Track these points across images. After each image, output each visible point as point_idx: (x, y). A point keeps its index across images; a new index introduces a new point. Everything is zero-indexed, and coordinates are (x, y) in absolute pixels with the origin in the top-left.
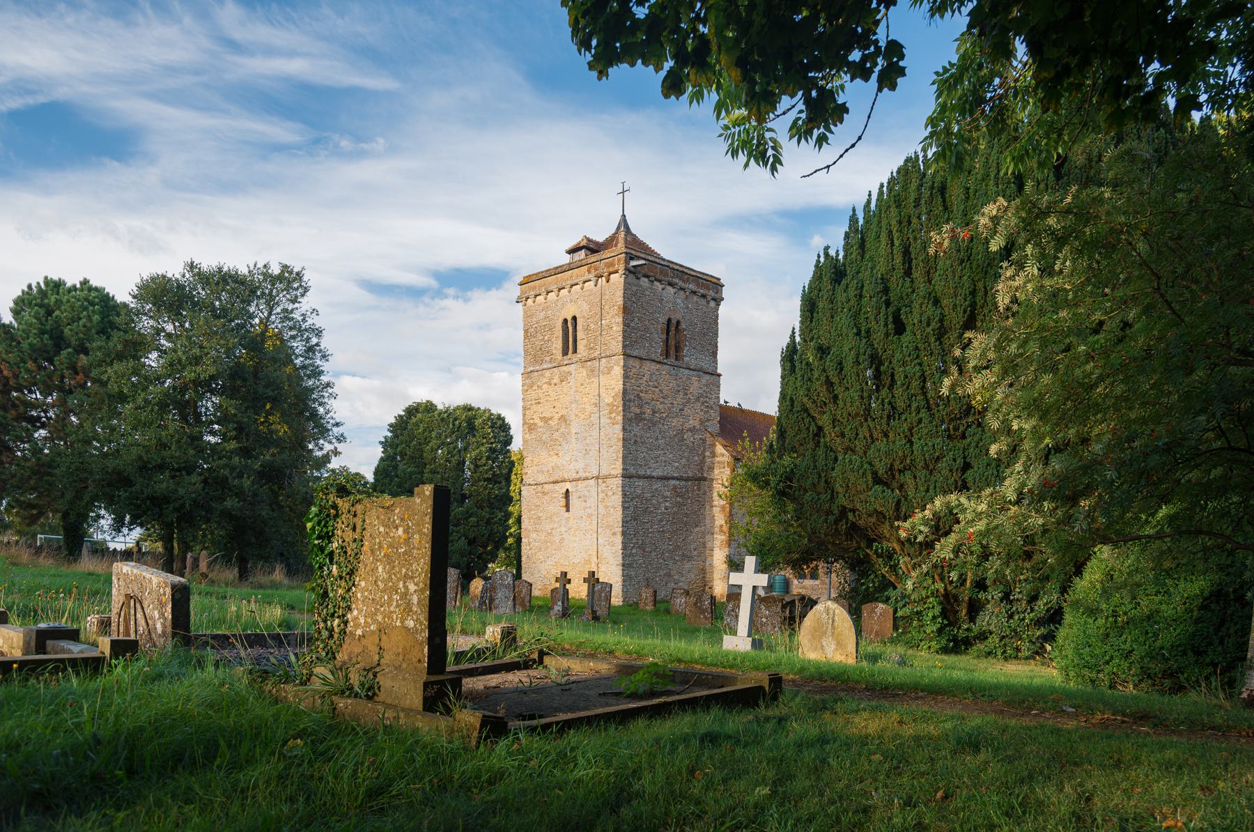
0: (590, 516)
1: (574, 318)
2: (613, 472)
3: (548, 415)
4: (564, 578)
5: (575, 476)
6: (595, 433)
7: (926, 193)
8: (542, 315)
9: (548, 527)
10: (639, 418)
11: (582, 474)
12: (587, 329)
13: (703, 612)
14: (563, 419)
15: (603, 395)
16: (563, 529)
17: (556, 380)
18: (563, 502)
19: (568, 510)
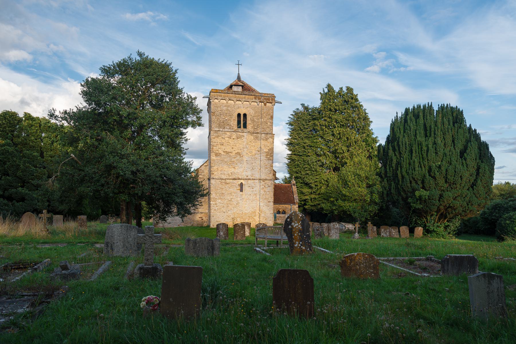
0: (256, 194)
1: (245, 115)
2: (268, 178)
3: (228, 150)
4: (341, 88)
5: (245, 177)
6: (258, 162)
7: (447, 133)
8: (225, 108)
9: (229, 198)
10: (340, 93)
11: (249, 177)
12: (253, 121)
13: (374, 232)
14: (238, 154)
15: (263, 148)
16: (239, 199)
17: (234, 137)
18: (239, 188)
19: (241, 190)
